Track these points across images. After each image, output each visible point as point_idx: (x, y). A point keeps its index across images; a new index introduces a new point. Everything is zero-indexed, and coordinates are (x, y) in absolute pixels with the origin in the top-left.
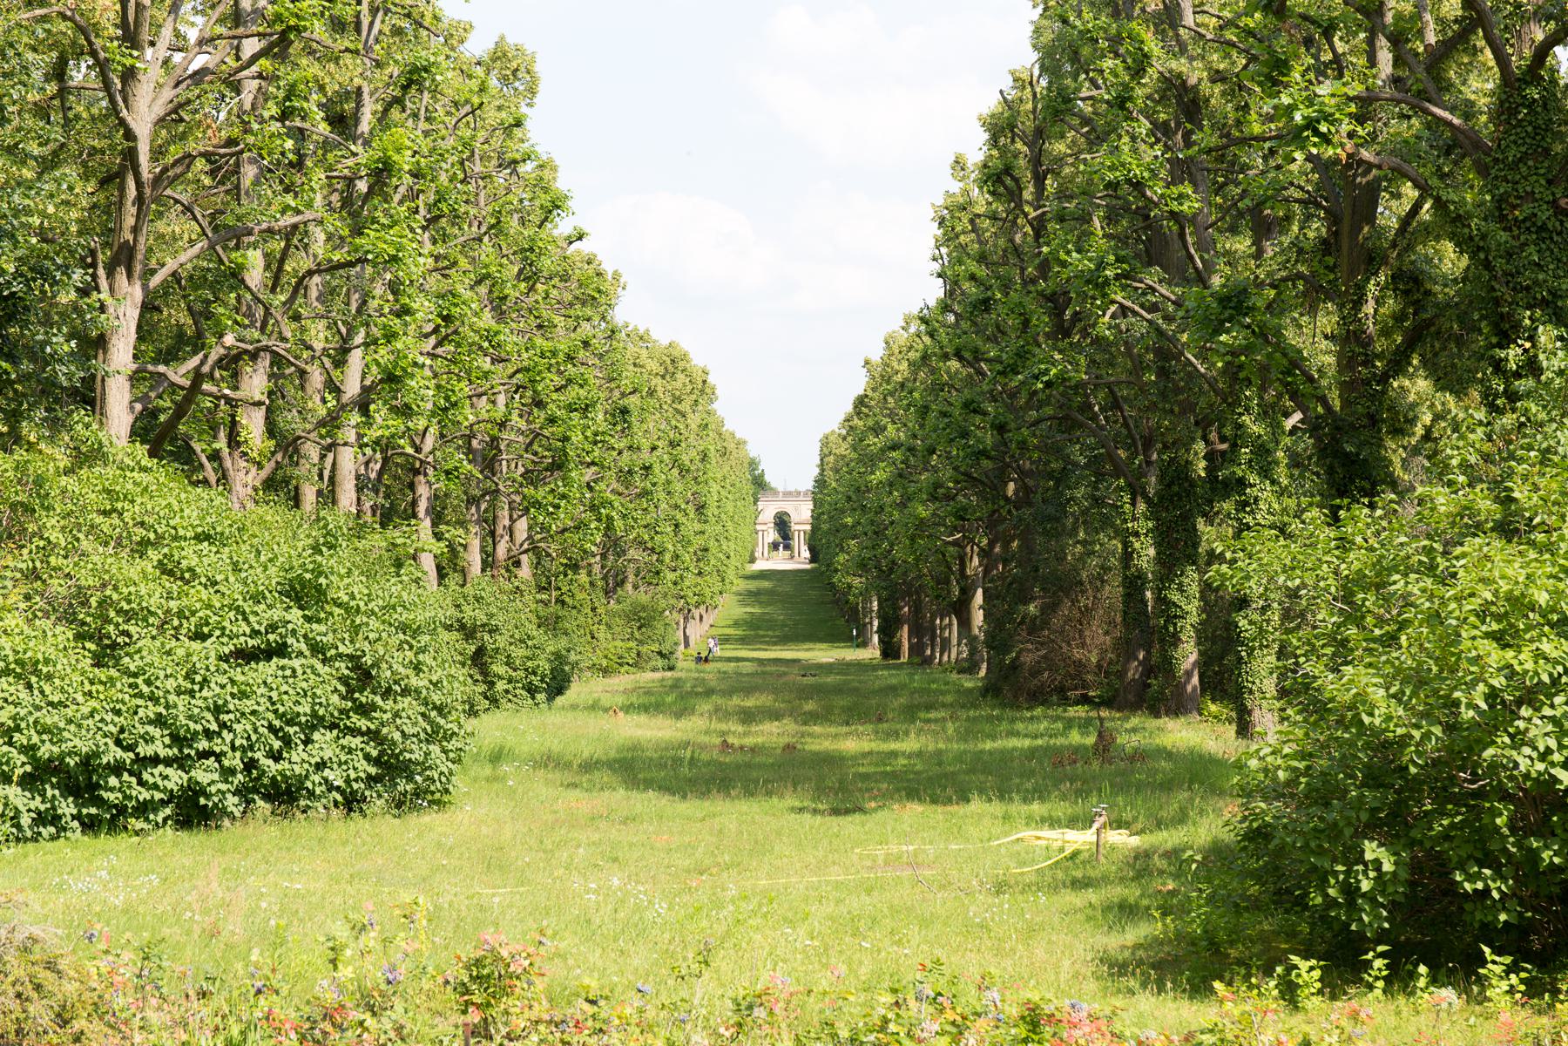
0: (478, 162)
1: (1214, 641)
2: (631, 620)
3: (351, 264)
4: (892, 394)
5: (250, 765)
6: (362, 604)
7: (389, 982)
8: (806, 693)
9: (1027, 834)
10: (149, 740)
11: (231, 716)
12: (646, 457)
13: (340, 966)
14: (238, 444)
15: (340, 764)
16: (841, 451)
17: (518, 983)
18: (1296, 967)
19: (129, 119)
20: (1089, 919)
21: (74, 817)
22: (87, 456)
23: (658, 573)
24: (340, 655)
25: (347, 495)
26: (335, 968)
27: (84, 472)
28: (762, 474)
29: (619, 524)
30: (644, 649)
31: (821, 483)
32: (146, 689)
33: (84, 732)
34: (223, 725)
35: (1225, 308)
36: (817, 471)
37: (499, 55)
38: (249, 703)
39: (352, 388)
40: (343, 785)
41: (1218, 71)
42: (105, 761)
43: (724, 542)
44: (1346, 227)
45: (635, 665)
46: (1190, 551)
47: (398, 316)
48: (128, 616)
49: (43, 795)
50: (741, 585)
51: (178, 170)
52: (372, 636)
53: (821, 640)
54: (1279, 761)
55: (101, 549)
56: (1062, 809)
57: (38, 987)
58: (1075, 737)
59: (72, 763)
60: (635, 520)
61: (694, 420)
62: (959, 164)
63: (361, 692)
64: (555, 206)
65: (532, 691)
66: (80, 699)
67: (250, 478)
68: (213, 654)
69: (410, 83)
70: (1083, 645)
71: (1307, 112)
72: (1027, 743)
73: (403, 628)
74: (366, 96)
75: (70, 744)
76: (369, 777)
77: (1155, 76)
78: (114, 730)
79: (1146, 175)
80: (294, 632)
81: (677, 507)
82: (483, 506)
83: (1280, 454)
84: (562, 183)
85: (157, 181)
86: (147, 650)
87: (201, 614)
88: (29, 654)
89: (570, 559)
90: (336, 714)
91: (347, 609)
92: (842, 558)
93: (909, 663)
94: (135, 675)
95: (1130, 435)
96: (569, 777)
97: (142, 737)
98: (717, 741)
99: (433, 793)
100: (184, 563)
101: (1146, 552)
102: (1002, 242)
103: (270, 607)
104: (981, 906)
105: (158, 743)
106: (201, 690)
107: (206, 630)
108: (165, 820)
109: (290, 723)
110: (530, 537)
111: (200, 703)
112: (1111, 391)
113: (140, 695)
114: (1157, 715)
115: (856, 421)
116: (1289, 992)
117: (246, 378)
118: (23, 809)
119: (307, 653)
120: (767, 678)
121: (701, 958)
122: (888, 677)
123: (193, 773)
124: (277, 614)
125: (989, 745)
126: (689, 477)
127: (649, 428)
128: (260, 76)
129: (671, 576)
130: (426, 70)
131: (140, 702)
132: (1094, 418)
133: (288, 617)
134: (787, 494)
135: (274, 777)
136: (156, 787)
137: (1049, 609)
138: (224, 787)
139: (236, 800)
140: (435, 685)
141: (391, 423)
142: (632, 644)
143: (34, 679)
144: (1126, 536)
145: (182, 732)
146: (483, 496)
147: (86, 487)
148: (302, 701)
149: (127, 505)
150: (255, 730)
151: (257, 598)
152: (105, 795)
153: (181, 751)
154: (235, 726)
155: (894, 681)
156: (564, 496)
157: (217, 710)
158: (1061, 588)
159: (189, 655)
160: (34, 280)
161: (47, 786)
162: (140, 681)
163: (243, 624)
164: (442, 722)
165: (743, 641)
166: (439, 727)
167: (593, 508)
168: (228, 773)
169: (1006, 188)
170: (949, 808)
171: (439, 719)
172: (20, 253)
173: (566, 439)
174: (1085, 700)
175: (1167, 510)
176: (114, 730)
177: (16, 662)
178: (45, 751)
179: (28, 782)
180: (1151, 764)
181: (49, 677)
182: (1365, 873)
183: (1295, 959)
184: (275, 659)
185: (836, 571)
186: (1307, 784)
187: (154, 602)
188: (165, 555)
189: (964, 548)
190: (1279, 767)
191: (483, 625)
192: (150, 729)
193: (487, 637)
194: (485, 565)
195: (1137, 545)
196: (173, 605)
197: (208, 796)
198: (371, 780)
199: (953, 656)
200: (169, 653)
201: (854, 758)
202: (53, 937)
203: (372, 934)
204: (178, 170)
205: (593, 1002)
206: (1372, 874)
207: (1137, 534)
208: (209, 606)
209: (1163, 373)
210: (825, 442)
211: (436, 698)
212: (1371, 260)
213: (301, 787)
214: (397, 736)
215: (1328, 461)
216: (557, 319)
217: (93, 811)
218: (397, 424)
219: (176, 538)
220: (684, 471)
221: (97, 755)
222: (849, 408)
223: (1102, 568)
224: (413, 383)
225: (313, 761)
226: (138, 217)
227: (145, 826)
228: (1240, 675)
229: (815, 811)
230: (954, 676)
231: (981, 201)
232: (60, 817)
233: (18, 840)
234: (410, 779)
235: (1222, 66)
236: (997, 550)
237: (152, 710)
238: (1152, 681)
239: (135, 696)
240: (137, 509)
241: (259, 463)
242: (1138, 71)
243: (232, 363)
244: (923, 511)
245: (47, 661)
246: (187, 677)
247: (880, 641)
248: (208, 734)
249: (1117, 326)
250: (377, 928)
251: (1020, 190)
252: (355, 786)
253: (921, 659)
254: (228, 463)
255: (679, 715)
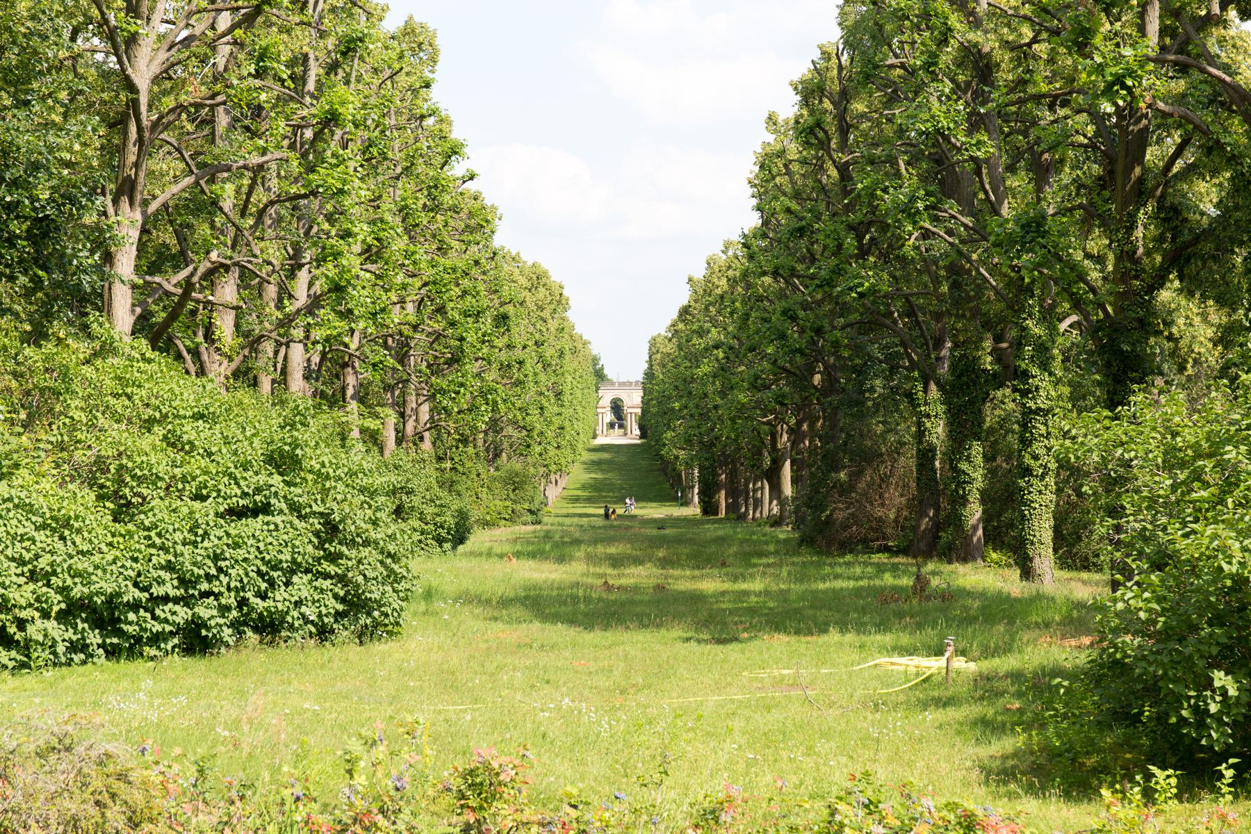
0: (393, 117)
1: (993, 501)
3: (305, 196)
5: (243, 603)
6: (331, 471)
7: (397, 789)
8: (656, 542)
9: (883, 660)
10: (161, 582)
11: (227, 563)
12: (518, 353)
13: (356, 776)
14: (213, 341)
15: (314, 602)
16: (668, 350)
17: (505, 789)
18: (1154, 775)
19: (133, 76)
20: (959, 733)
21: (99, 646)
22: (106, 349)
23: (528, 446)
24: (315, 513)
25: (297, 383)
26: (352, 777)
27: (99, 362)
28: (602, 368)
30: (518, 507)
31: (649, 375)
32: (158, 541)
33: (108, 576)
34: (220, 570)
35: (1028, 233)
36: (646, 366)
37: (409, 31)
38: (241, 552)
41: (1007, 42)
42: (125, 600)
43: (575, 422)
44: (1120, 167)
46: (976, 429)
47: (342, 238)
48: (140, 480)
49: (75, 627)
50: (586, 456)
51: (171, 117)
52: (339, 497)
54: (1141, 604)
55: (116, 426)
57: (113, 796)
59: (99, 602)
61: (553, 325)
62: (771, 120)
63: (330, 544)
64: (454, 151)
65: (440, 541)
66: (105, 549)
67: (222, 369)
68: (212, 513)
70: (883, 505)
72: (852, 584)
75: (97, 586)
78: (133, 574)
81: (541, 394)
82: (397, 393)
83: (1056, 351)
84: (456, 134)
85: (155, 125)
87: (200, 479)
88: (63, 512)
89: (462, 435)
90: (310, 561)
91: (319, 474)
92: (669, 434)
93: (727, 519)
94: (148, 529)
96: (490, 612)
97: (155, 580)
98: (600, 582)
99: (386, 625)
100: (185, 437)
101: (938, 431)
103: (257, 473)
104: (867, 721)
105: (168, 585)
107: (204, 492)
108: (173, 647)
109: (274, 568)
110: (432, 417)
111: (202, 552)
112: (908, 300)
113: (153, 545)
114: (950, 562)
115: (681, 326)
116: (1149, 795)
118: (59, 639)
119: (287, 511)
121: (661, 769)
122: (712, 530)
123: (196, 610)
124: (262, 479)
127: (520, 330)
128: (235, 43)
129: (538, 449)
130: (361, 40)
131: (153, 551)
132: (895, 322)
133: (271, 482)
134: (623, 384)
136: (166, 621)
137: (856, 475)
138: (221, 621)
139: (230, 631)
142: (508, 503)
143: (67, 533)
145: (188, 576)
147: (103, 374)
149: (135, 390)
150: (247, 574)
151: (246, 466)
152: (125, 627)
153: (186, 591)
155: (721, 533)
156: (462, 385)
157: (216, 558)
159: (191, 513)
160: (64, 205)
161: (78, 621)
162: (153, 534)
163: (235, 487)
164: (396, 567)
168: (224, 609)
169: (817, 138)
172: (54, 182)
174: (885, 549)
175: (958, 396)
176: (133, 574)
177: (52, 518)
178: (78, 591)
179: (65, 617)
180: (961, 602)
181: (79, 531)
182: (1213, 698)
183: (1154, 769)
184: (261, 517)
185: (664, 445)
186: (1164, 623)
187: (161, 469)
188: (169, 431)
189: (775, 426)
191: (402, 488)
192: (162, 573)
193: (404, 497)
194: (399, 441)
195: (928, 425)
196: (177, 471)
197: (208, 629)
198: (339, 615)
199: (766, 513)
200: (174, 511)
201: (714, 595)
202: (124, 754)
203: (381, 748)
204: (171, 117)
205: (575, 807)
206: (1218, 699)
207: (928, 416)
208: (206, 473)
209: (955, 286)
210: (653, 343)
211: (392, 548)
212: (1140, 193)
213: (283, 621)
214: (360, 579)
215: (1106, 357)
216: (455, 244)
217: (115, 641)
218: (342, 325)
219: (176, 416)
220: (546, 366)
221: (119, 595)
222: (675, 315)
223: (899, 442)
225: (293, 600)
226: (139, 156)
227: (157, 653)
228: (1023, 529)
230: (768, 529)
232: (88, 646)
233: (55, 664)
234: (369, 614)
235: (1011, 38)
236: (805, 427)
237: (163, 558)
238: (942, 534)
239: (149, 546)
240: (144, 393)
242: (943, 42)
244: (743, 397)
245: (77, 518)
246: (190, 530)
248: (209, 578)
250: (385, 743)
251: (829, 140)
252: (326, 620)
254: (205, 357)
255: (561, 559)
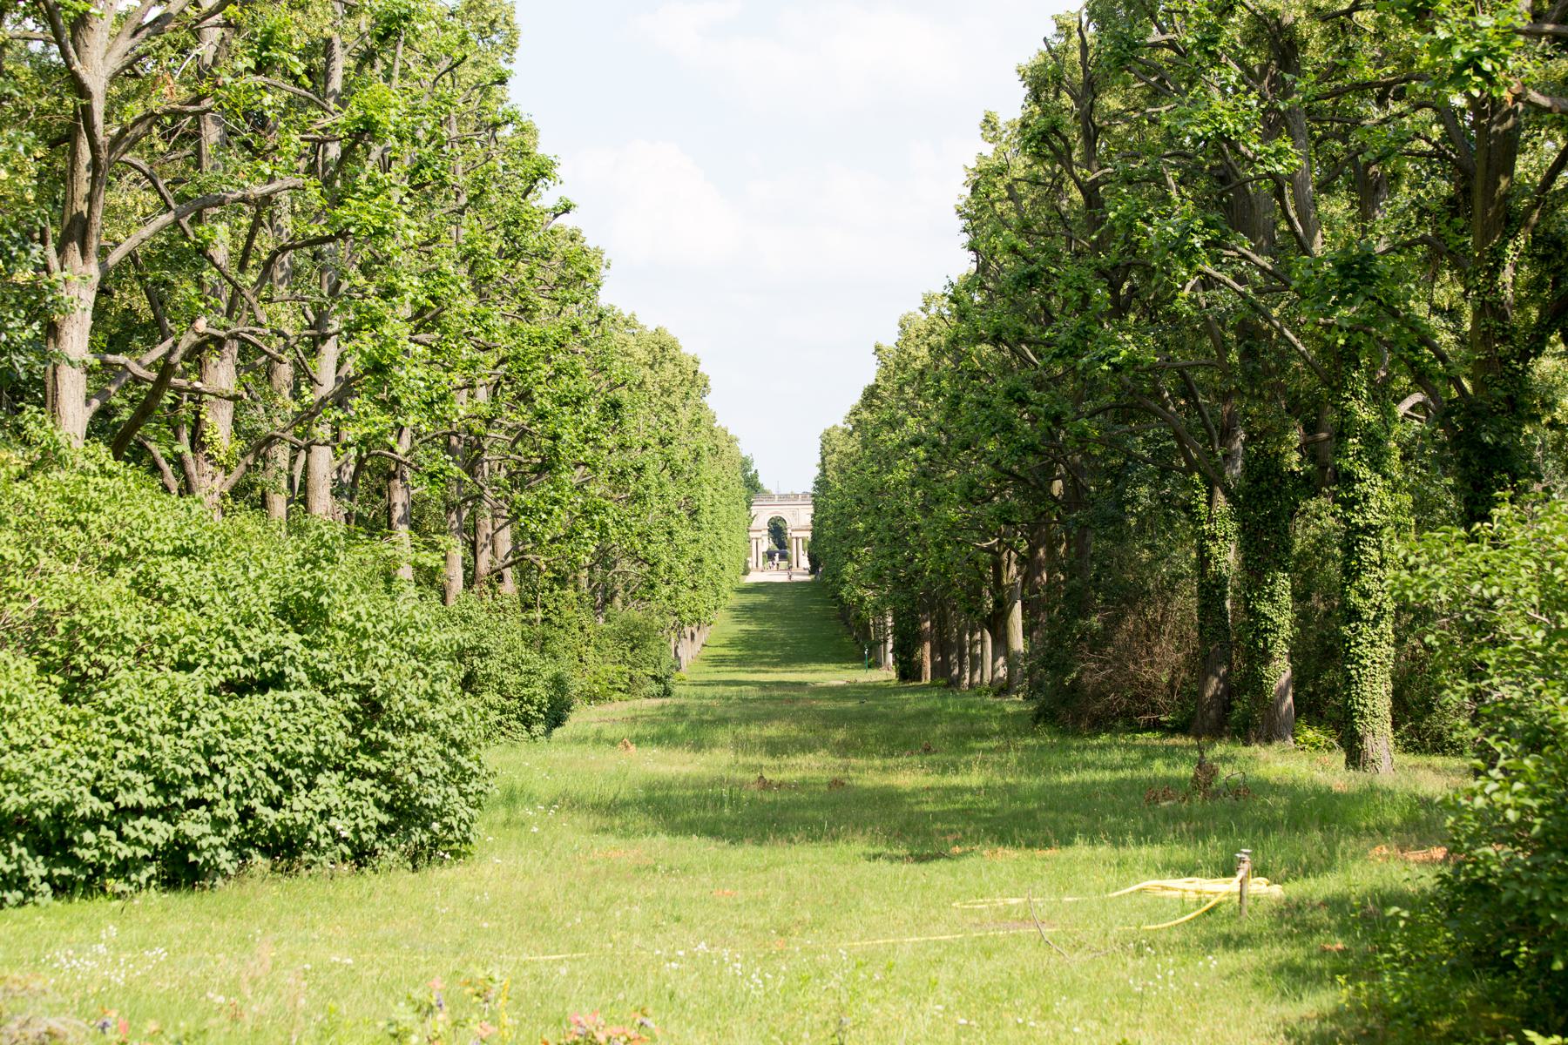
0: (454, 125)
4: (907, 383)
5: (246, 814)
6: (369, 626)
8: (839, 719)
9: (1151, 883)
10: (129, 787)
11: (224, 758)
12: (636, 456)
14: (203, 445)
15: (347, 812)
19: (82, 73)
20: (1257, 984)
21: (43, 879)
23: (652, 587)
24: (347, 686)
30: (637, 673)
31: (822, 484)
32: (125, 729)
33: (55, 779)
34: (214, 768)
35: (1346, 277)
36: (818, 471)
38: (243, 742)
39: (328, 383)
40: (351, 837)
42: (80, 813)
44: (1478, 185)
47: (384, 297)
48: (100, 643)
50: (735, 600)
52: (382, 663)
53: (826, 661)
54: (1508, 800)
55: (64, 567)
56: (1182, 853)
58: (1159, 768)
59: (42, 817)
61: (685, 415)
63: (370, 729)
64: (541, 173)
65: (527, 721)
66: (50, 741)
69: (389, 32)
71: (1466, 47)
72: (1107, 776)
73: (414, 653)
74: (337, 49)
75: (40, 794)
76: (381, 826)
77: (1246, 14)
78: (90, 776)
79: (1240, 128)
80: (292, 659)
81: (670, 512)
82: (465, 514)
84: (544, 148)
85: (115, 142)
86: (127, 684)
87: (186, 640)
89: (558, 572)
90: (342, 753)
91: (352, 630)
92: (850, 568)
94: (112, 712)
95: (1205, 425)
97: (122, 784)
98: (753, 777)
99: (450, 843)
100: (163, 582)
101: (1228, 558)
102: (1043, 210)
103: (265, 631)
105: (141, 790)
106: (188, 728)
107: (191, 658)
108: (149, 880)
111: (188, 743)
112: (1183, 375)
113: (119, 735)
114: (1247, 743)
115: (866, 415)
117: (210, 368)
119: (308, 684)
120: (778, 702)
122: (912, 702)
123: (181, 825)
124: (273, 639)
125: (1065, 779)
126: (681, 479)
127: (639, 424)
128: (228, 24)
129: (666, 590)
130: (406, 18)
131: (119, 743)
133: (285, 643)
135: (273, 828)
136: (138, 842)
137: (1114, 622)
138: (216, 840)
139: (229, 854)
140: (454, 717)
141: (378, 419)
142: (624, 668)
144: (1203, 541)
145: (168, 778)
146: (465, 501)
148: (305, 738)
149: (91, 516)
150: (252, 774)
153: (166, 799)
154: (228, 769)
155: (924, 706)
156: (556, 502)
157: (208, 751)
158: (1126, 600)
159: (172, 688)
161: (13, 844)
162: (118, 719)
164: (463, 760)
165: (740, 662)
166: (458, 765)
167: (586, 514)
168: (220, 824)
170: (1048, 853)
171: (459, 758)
173: (555, 437)
176: (90, 776)
184: (271, 692)
185: (844, 582)
186: (1543, 826)
187: (130, 628)
188: (140, 573)
189: (999, 554)
190: (1508, 806)
191: (473, 649)
192: (132, 774)
193: (476, 661)
195: (1215, 550)
197: (198, 852)
200: (149, 686)
201: (914, 793)
203: (440, 1017)
207: (1214, 538)
208: (193, 631)
209: (1248, 354)
210: (826, 439)
211: (457, 733)
212: (1510, 222)
214: (413, 778)
217: (66, 871)
218: (385, 420)
221: (70, 806)
222: (856, 398)
224: (403, 374)
225: (318, 809)
227: (126, 887)
228: (1349, 696)
229: (892, 859)
230: (990, 699)
231: (1020, 165)
232: (27, 880)
234: (425, 827)
237: (132, 753)
239: (112, 736)
240: (103, 520)
241: (226, 467)
243: (196, 353)
244: (952, 514)
246: (172, 713)
249: (1196, 301)
250: (447, 1009)
252: (365, 837)
253: (946, 679)
255: (698, 746)
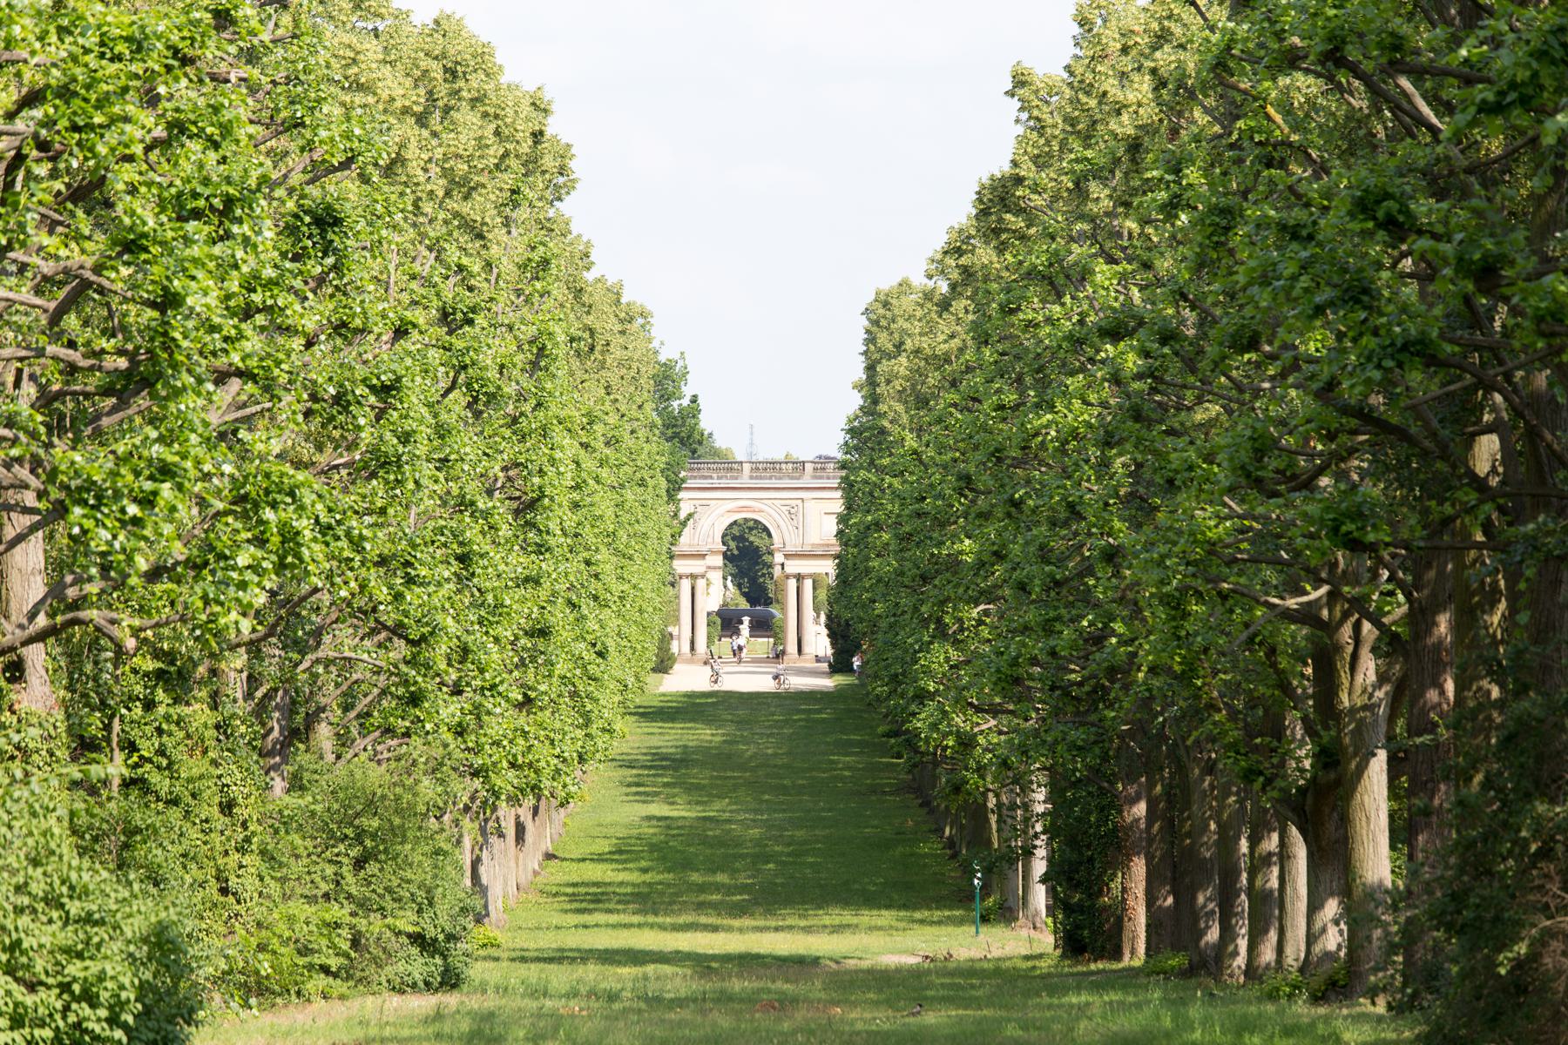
2: (333, 839)
4: (1099, 174)
12: (379, 357)
23: (415, 700)
29: (313, 551)
30: (373, 926)
36: (856, 401)
43: (587, 607)
45: (343, 974)
50: (634, 737)
60: (357, 544)
61: (507, 249)
81: (464, 504)
92: (940, 656)
115: (985, 255)
126: (496, 417)
129: (451, 710)
156: (165, 471)
165: (645, 901)
173: (168, 301)
185: (922, 696)
189: (1330, 628)
220: (481, 401)
222: (962, 212)
247: (1057, 904)
